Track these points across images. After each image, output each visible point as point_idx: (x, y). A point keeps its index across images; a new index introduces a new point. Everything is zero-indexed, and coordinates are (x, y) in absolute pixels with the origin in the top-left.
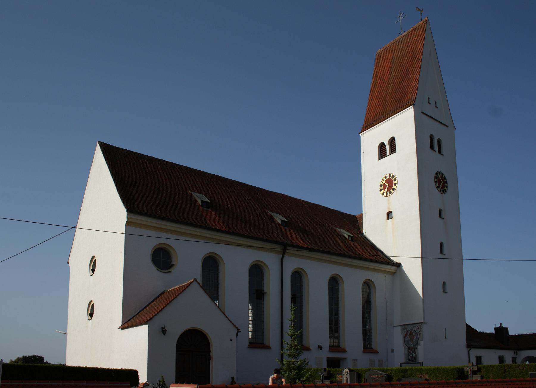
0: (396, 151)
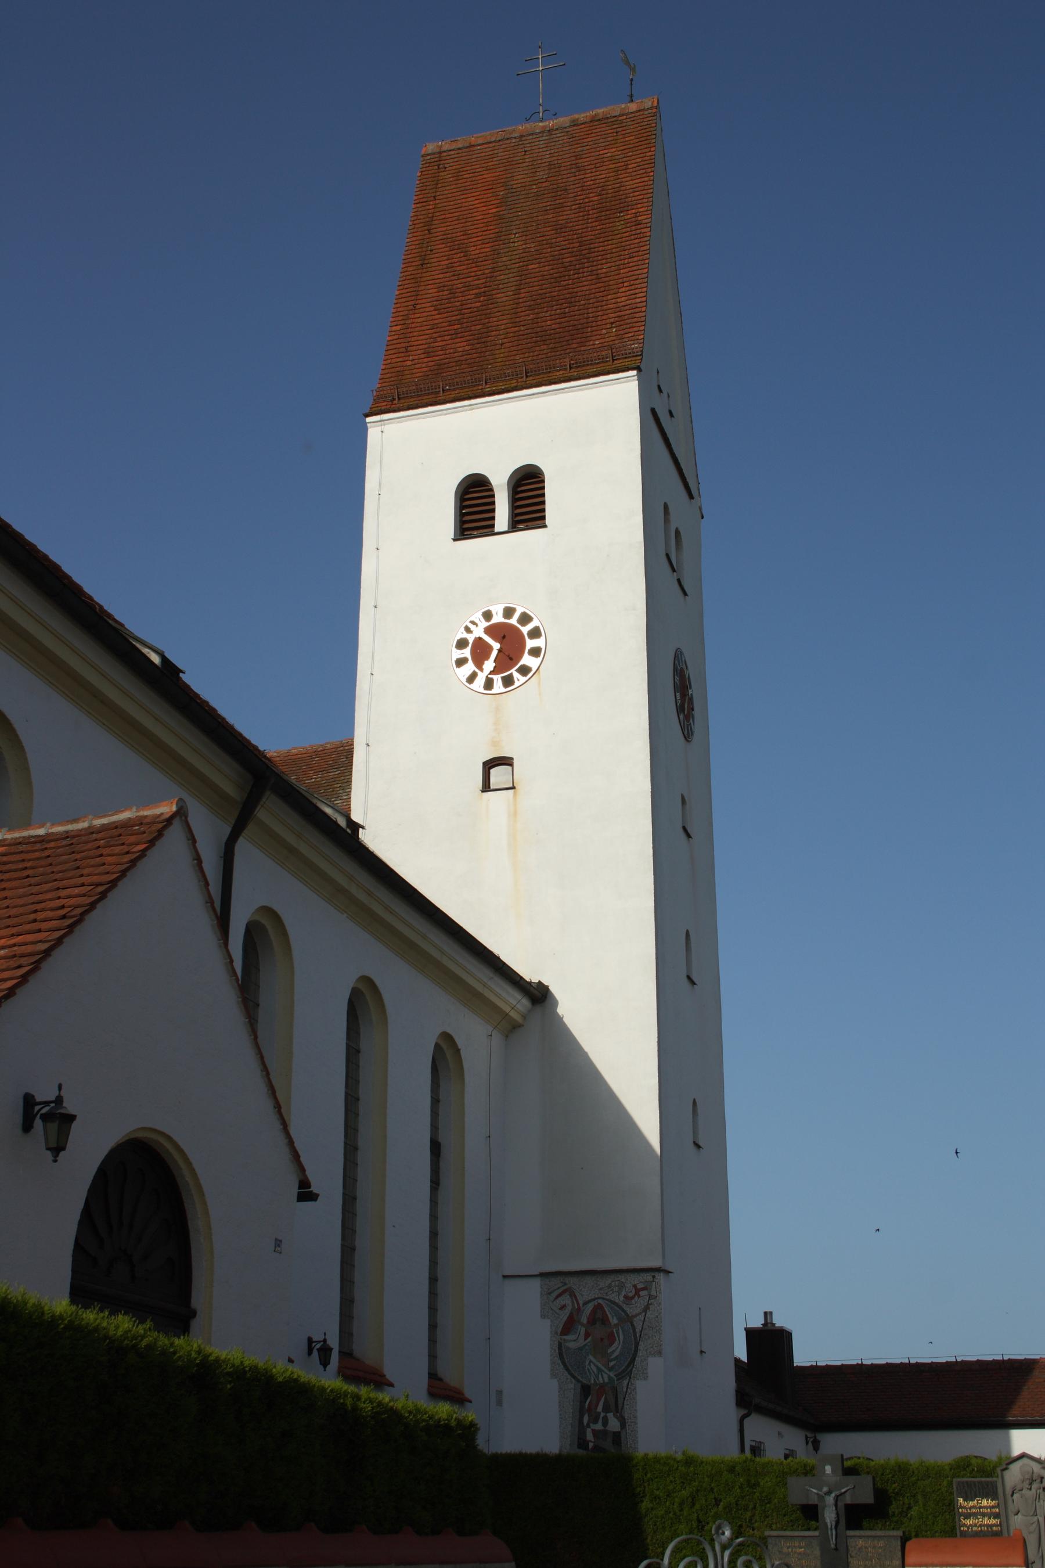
0: (548, 521)
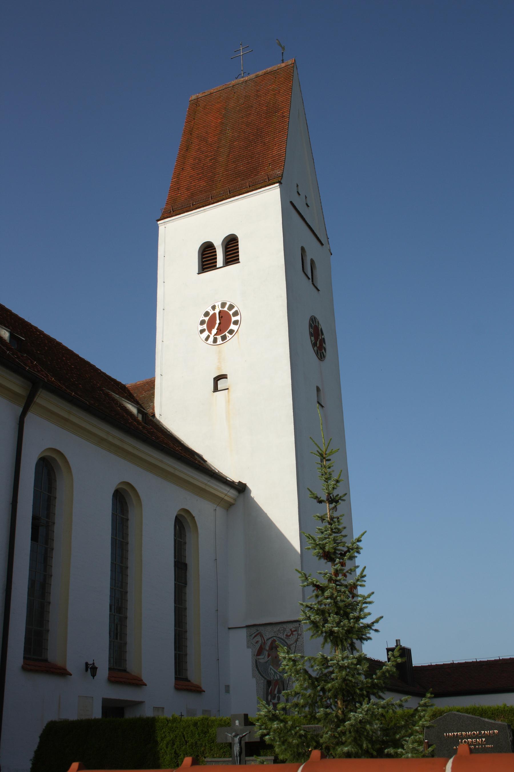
0: (240, 260)
